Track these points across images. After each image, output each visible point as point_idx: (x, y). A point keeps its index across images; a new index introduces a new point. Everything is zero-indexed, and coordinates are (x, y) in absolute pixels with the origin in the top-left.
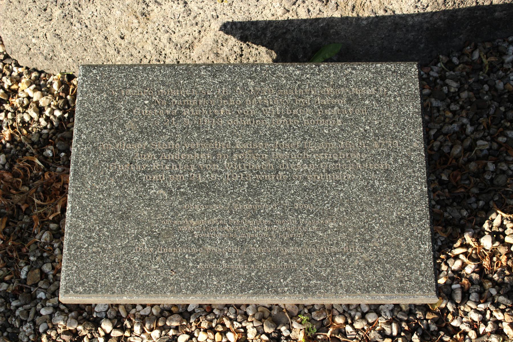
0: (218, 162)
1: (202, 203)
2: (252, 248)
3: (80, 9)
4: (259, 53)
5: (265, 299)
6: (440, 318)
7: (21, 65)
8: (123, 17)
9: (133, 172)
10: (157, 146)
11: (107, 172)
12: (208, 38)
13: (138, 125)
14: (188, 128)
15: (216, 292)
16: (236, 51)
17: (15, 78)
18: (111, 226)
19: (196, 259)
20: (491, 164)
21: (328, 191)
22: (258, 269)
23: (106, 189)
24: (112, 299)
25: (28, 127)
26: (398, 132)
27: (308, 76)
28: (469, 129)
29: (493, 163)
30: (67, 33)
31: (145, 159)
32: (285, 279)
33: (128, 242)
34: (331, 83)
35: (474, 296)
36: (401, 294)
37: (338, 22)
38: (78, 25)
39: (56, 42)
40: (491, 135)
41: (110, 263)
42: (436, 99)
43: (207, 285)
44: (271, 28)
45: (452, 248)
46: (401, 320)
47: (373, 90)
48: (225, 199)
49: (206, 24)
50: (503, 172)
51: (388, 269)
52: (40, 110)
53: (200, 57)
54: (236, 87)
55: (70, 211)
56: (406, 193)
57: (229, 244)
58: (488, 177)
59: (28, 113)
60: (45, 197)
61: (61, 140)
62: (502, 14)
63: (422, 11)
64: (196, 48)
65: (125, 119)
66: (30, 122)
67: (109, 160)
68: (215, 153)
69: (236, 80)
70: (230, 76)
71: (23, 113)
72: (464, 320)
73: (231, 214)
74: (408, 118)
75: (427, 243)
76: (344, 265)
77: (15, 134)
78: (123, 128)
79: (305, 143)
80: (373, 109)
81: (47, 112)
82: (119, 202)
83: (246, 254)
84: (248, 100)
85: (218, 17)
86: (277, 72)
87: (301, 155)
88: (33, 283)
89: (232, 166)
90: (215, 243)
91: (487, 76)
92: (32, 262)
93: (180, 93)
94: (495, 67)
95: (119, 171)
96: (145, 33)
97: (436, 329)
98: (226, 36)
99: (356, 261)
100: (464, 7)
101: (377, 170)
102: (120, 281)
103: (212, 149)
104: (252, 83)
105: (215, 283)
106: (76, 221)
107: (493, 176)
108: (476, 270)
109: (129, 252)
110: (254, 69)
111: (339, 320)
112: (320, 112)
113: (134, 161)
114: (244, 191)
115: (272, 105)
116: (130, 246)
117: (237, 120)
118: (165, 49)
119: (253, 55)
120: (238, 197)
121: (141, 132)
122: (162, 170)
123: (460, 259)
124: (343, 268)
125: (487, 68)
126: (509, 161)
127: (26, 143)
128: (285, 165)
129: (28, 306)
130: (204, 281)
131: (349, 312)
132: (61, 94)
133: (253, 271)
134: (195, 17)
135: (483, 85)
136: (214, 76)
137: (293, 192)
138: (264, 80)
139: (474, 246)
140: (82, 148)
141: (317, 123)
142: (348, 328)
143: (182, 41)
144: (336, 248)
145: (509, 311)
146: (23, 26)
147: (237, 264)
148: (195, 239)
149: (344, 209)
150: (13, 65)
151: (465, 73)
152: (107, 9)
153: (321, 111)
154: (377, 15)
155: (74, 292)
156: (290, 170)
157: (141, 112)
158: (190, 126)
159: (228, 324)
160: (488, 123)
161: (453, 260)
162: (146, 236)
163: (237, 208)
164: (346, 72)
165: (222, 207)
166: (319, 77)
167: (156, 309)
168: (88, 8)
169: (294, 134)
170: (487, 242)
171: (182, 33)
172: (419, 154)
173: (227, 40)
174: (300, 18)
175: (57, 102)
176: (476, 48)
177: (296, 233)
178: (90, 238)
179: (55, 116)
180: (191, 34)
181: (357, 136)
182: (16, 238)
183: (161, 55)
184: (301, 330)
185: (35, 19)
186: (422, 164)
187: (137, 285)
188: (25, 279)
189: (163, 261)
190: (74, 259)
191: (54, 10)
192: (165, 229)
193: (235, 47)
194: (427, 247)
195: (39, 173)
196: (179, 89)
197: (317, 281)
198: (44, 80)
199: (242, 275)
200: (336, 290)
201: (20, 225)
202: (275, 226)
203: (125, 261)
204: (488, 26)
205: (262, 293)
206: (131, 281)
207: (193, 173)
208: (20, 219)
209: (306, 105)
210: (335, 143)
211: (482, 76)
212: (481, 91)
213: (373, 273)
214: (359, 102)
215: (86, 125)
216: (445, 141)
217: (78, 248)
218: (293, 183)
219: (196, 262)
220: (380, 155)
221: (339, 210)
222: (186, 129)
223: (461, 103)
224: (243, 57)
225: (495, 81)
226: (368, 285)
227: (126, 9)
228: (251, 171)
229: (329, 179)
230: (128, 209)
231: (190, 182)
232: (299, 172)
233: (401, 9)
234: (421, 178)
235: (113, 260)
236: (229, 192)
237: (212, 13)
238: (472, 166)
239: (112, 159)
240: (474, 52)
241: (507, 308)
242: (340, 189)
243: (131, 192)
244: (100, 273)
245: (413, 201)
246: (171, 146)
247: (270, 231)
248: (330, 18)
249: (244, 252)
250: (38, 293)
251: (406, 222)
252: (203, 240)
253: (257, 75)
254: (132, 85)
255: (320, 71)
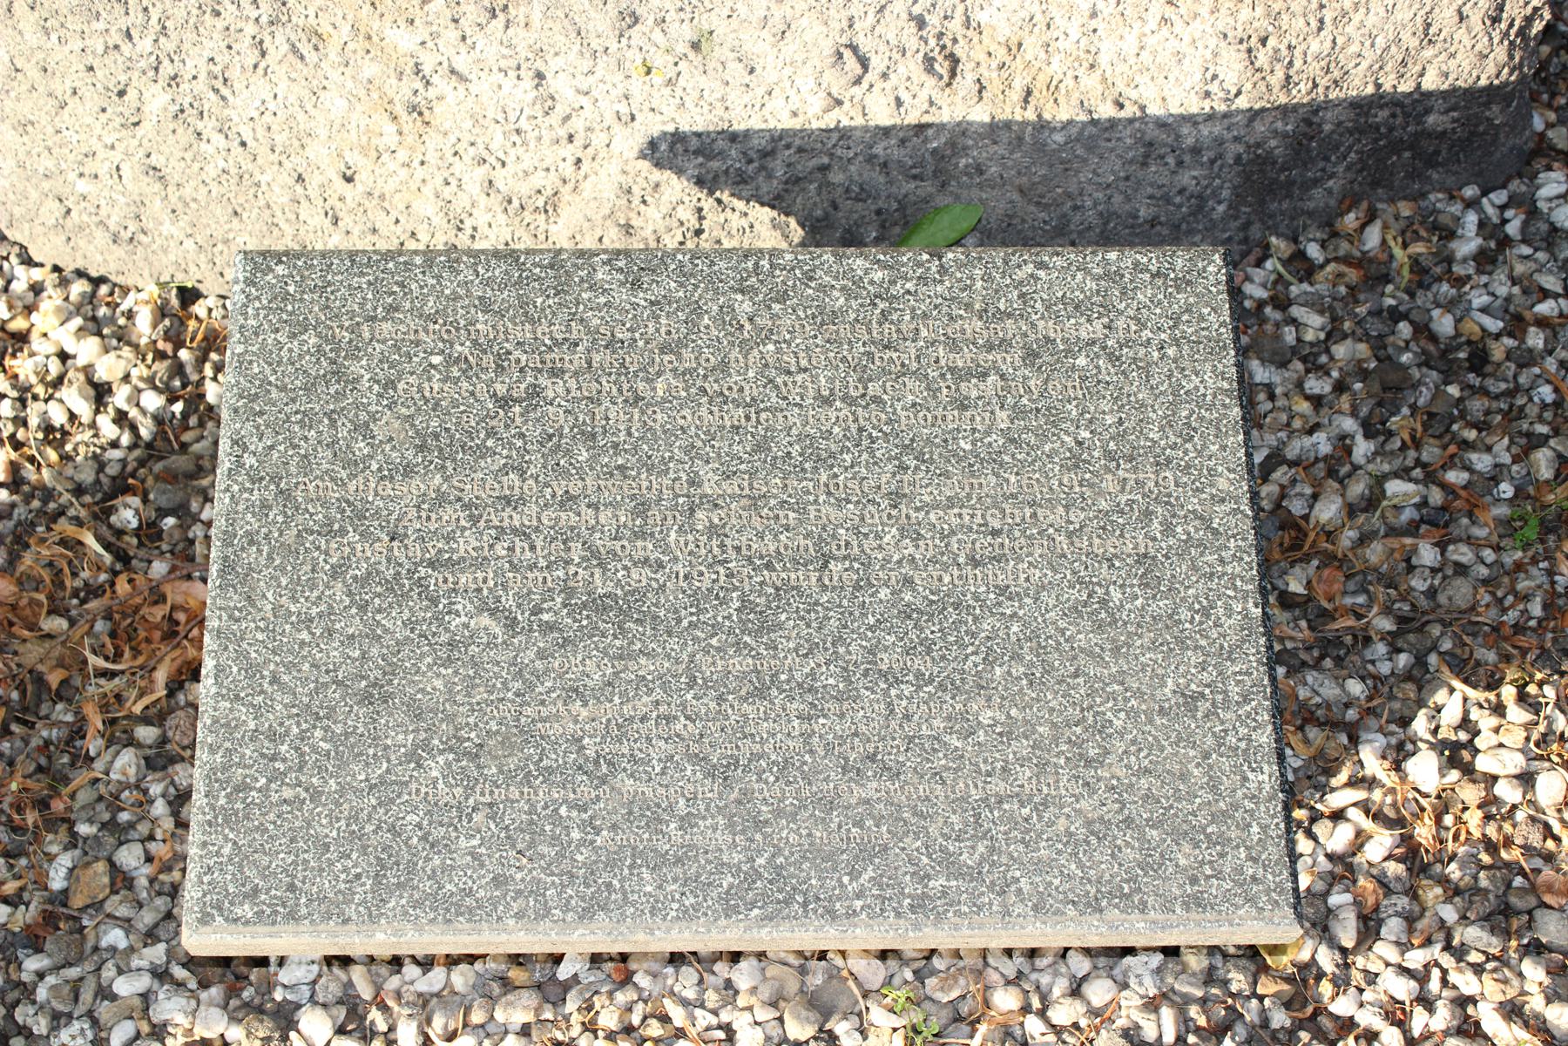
0: (652, 535)
1: (606, 654)
2: (756, 786)
3: (225, 91)
4: (752, 227)
5: (797, 934)
6: (1296, 993)
7: (37, 259)
8: (355, 116)
9: (400, 565)
10: (469, 486)
11: (322, 563)
12: (603, 182)
13: (413, 425)
14: (561, 436)
15: (653, 914)
16: (683, 219)
17: (20, 298)
18: (335, 722)
19: (591, 818)
20: (1428, 546)
21: (976, 619)
22: (774, 846)
23: (320, 615)
24: (341, 940)
25: (62, 443)
26: (1174, 447)
27: (908, 285)
28: (1362, 448)
29: (1436, 545)
30: (183, 164)
31: (433, 526)
32: (854, 875)
33: (388, 771)
34: (977, 306)
35: (1393, 927)
36: (1193, 915)
37: (982, 136)
38: (218, 139)
39: (148, 190)
40: (1424, 466)
41: (334, 833)
42: (1263, 361)
43: (625, 894)
44: (787, 153)
45: (1324, 789)
46: (1188, 1000)
47: (1098, 325)
48: (673, 644)
49: (599, 139)
50: (1461, 570)
51: (1154, 844)
52: (100, 393)
53: (578, 238)
54: (700, 316)
55: (211, 681)
56: (1201, 623)
57: (689, 772)
58: (1419, 584)
59: (61, 401)
60: (116, 647)
61: (166, 481)
62: (1445, 118)
63: (1223, 108)
64: (564, 211)
65: (373, 408)
66: (67, 427)
67: (328, 530)
68: (642, 509)
69: (701, 297)
70: (681, 285)
71: (46, 401)
72: (1368, 996)
73: (692, 683)
74: (1200, 408)
75: (1266, 768)
76: (1028, 831)
77: (22, 461)
78: (369, 436)
79: (906, 478)
80: (1099, 382)
81: (120, 398)
82: (357, 653)
83: (739, 802)
84: (735, 353)
85: (633, 118)
86: (819, 272)
87: (894, 512)
88: (89, 901)
89: (691, 546)
90: (646, 772)
91: (1406, 297)
92: (85, 839)
93: (534, 332)
94: (1426, 271)
95: (358, 562)
96: (416, 163)
97: (1288, 1023)
98: (657, 175)
99: (1062, 820)
100: (1342, 95)
101: (1115, 555)
102: (364, 884)
103: (633, 497)
104: (747, 307)
105: (649, 889)
106: (231, 710)
107: (1436, 582)
108: (1397, 851)
109: (392, 801)
110: (750, 264)
111: (1006, 1000)
112: (945, 391)
113: (402, 531)
114: (729, 617)
115: (805, 370)
116: (395, 783)
117: (704, 411)
118: (474, 211)
119: (734, 232)
120: (712, 636)
121: (422, 448)
122: (485, 559)
123: (1348, 820)
124: (1023, 841)
125: (1406, 272)
126: (1477, 539)
127: (59, 488)
128: (847, 544)
129: (73, 972)
130: (615, 882)
131: (1034, 976)
132: (161, 345)
133: (759, 852)
134: (567, 118)
135: (1396, 322)
136: (636, 285)
137: (871, 620)
138: (782, 298)
139: (1389, 784)
140: (246, 495)
141: (939, 422)
142: (1033, 1025)
143: (525, 188)
144: (1002, 784)
145: (1495, 970)
146: (50, 143)
147: (714, 835)
148: (587, 759)
149: (1022, 669)
150: (14, 259)
151: (1343, 290)
152: (306, 93)
153: (948, 387)
154: (1096, 116)
155: (227, 920)
156: (863, 559)
157: (420, 390)
158: (566, 430)
159: (678, 1016)
160: (1414, 430)
161: (1329, 824)
162: (442, 752)
163: (708, 667)
164: (1020, 275)
165: (666, 665)
166: (939, 291)
167: (462, 974)
168: (252, 88)
169: (872, 453)
170: (1425, 770)
171: (527, 164)
172: (1235, 511)
173: (657, 185)
174: (872, 123)
175: (149, 367)
176: (1371, 217)
177: (883, 739)
178: (273, 759)
179: (144, 412)
180: (553, 169)
181: (1056, 460)
182: (32, 768)
183: (460, 229)
184: (895, 1030)
185: (89, 120)
186: (1244, 539)
187: (416, 896)
188: (65, 891)
189: (492, 826)
190: (226, 821)
191: (146, 95)
192: (498, 732)
193: (680, 208)
194: (1265, 778)
195: (96, 578)
196: (533, 322)
197: (948, 880)
198: (108, 304)
199: (728, 865)
200: (1004, 905)
201: (45, 733)
202: (821, 721)
203: (379, 827)
204: (1407, 154)
205: (788, 917)
206: (399, 885)
207: (578, 565)
208: (42, 714)
209: (905, 371)
210: (993, 480)
211: (1394, 297)
212: (1391, 339)
213: (1113, 855)
214: (1058, 361)
215: (258, 428)
216: (1294, 482)
217: (237, 789)
218: (871, 596)
219: (591, 826)
220: (1122, 512)
221: (1009, 673)
222: (555, 439)
223: (1335, 374)
224: (703, 236)
225: (1429, 311)
226: (1098, 891)
227: (362, 93)
228: (749, 559)
229: (977, 584)
230: (385, 674)
231: (569, 592)
232: (889, 562)
233: (1164, 99)
234: (1242, 579)
235: (343, 822)
236: (685, 623)
237: (617, 107)
238: (1375, 553)
239: (336, 526)
240: (1368, 229)
241: (1488, 960)
242: (1008, 612)
243: (394, 623)
244: (305, 861)
245: (1222, 647)
246: (511, 488)
247: (807, 736)
248: (959, 124)
249: (733, 796)
250: (105, 933)
251: (1203, 706)
252: (610, 763)
253: (762, 282)
254: (393, 308)
255: (943, 270)
